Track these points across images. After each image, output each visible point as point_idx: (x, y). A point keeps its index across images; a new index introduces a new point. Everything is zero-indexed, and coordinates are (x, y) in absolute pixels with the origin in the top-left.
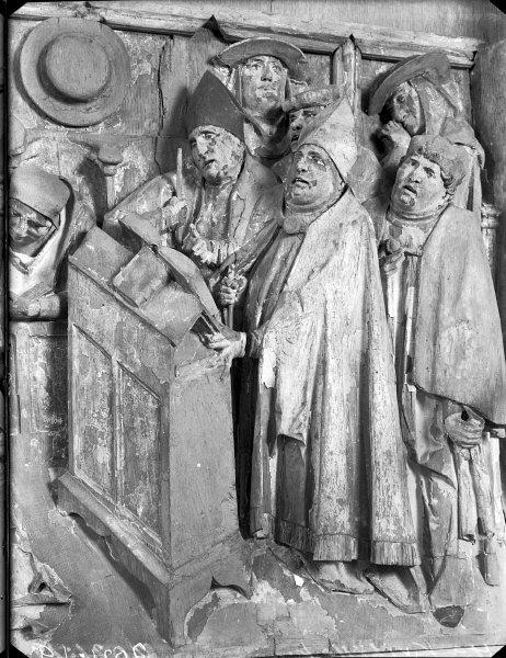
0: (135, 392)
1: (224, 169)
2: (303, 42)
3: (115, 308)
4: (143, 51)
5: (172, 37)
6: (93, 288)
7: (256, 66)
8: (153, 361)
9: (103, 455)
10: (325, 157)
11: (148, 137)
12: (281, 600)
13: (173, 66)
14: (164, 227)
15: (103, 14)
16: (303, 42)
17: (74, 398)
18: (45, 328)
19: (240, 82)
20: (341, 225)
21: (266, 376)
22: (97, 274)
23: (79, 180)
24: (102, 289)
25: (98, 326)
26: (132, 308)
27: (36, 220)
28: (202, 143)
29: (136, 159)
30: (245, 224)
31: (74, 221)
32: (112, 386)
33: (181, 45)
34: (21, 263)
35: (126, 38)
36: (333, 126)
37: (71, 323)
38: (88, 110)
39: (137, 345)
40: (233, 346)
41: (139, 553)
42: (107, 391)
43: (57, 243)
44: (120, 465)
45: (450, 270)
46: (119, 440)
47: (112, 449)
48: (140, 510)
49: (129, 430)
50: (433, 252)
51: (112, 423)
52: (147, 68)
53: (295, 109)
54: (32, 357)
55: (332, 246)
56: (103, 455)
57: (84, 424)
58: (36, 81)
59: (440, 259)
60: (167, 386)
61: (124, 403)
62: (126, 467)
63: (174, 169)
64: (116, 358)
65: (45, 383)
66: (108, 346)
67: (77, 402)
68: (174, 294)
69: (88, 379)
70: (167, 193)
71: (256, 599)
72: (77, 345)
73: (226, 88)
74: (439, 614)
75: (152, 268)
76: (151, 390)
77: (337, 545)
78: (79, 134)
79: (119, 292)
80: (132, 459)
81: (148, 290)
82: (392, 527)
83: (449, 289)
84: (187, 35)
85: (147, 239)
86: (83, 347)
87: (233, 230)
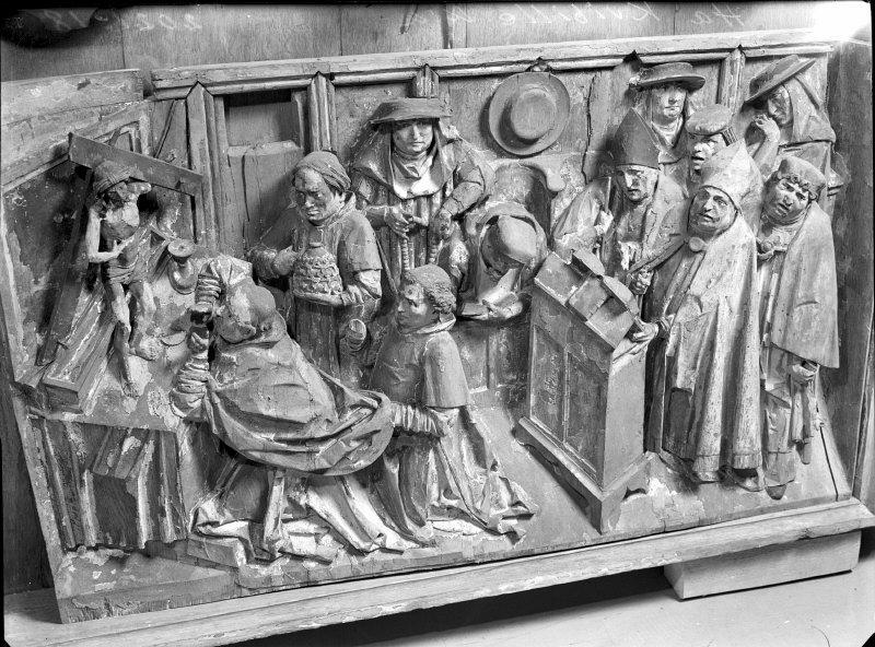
10: (726, 199)
12: (667, 492)
20: (733, 247)
21: (669, 350)
30: (656, 232)
36: (734, 171)
40: (649, 331)
41: (579, 476)
44: (566, 416)
45: (805, 264)
46: (567, 402)
48: (580, 448)
50: (795, 251)
55: (726, 264)
56: (552, 410)
58: (500, 114)
59: (800, 254)
62: (570, 419)
64: (567, 350)
71: (651, 493)
77: (708, 468)
80: (575, 415)
82: (748, 445)
83: (804, 277)
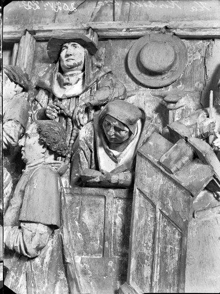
0: (168, 229)
3: (160, 176)
4: (197, 48)
5: (213, 40)
6: (149, 165)
8: (181, 206)
9: (147, 272)
11: (197, 91)
14: (199, 133)
15: (174, 31)
17: (133, 233)
18: (122, 193)
22: (152, 157)
23: (156, 116)
24: (154, 166)
25: (150, 188)
26: (169, 174)
27: (118, 126)
29: (188, 102)
31: (145, 131)
32: (155, 226)
34: (113, 155)
35: (187, 43)
37: (135, 187)
38: (162, 79)
39: (171, 198)
42: (152, 229)
43: (135, 144)
46: (157, 260)
47: (152, 268)
49: (164, 254)
51: (153, 250)
52: (198, 56)
54: (114, 210)
57: (138, 251)
60: (187, 223)
61: (162, 236)
62: (160, 280)
63: (208, 106)
64: (158, 207)
65: (121, 226)
66: (154, 199)
67: (134, 237)
68: (197, 166)
69: (142, 222)
70: (204, 117)
72: (138, 200)
75: (184, 150)
76: (177, 226)
78: (157, 92)
79: (163, 166)
81: (180, 163)
85: (182, 134)
86: (141, 202)
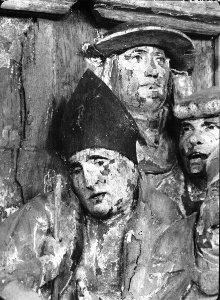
1: (118, 203)
2: (186, 25)
5: (35, 21)
7: (137, 57)
13: (38, 57)
16: (186, 25)
19: (116, 75)
28: (91, 171)
33: (48, 29)
53: (193, 118)
73: (100, 81)
74: (42, 254)
84: (54, 17)
87: (127, 280)
